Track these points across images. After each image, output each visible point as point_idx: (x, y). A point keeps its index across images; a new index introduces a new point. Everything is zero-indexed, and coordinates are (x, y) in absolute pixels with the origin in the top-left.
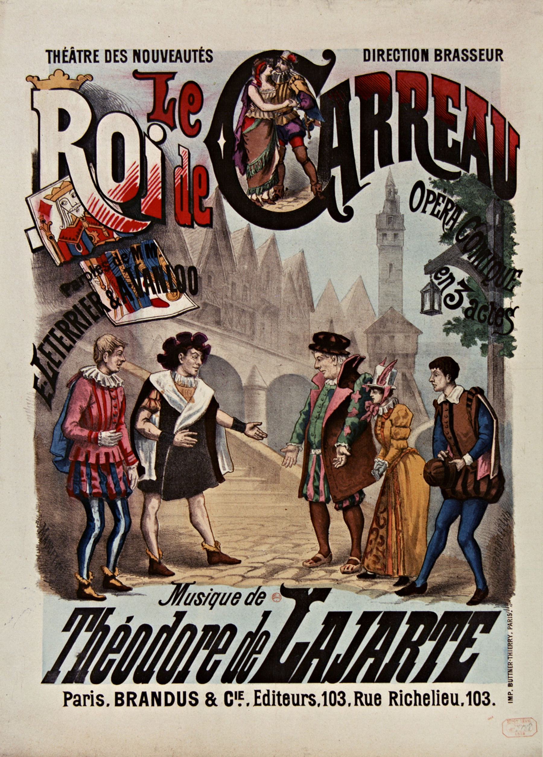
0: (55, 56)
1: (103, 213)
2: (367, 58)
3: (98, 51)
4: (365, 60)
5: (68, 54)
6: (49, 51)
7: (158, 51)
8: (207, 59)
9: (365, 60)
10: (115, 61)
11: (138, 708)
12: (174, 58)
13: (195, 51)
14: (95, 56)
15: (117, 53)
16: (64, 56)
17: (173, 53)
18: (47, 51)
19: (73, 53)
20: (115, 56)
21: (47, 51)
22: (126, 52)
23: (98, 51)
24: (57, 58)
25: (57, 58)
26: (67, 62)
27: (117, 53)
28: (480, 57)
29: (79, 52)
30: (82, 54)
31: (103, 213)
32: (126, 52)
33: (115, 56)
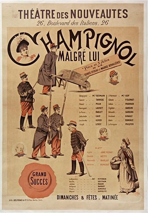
0: (25, 14)
1: (26, 105)
2: (59, 17)
3: (54, 10)
4: (58, 199)
5: (34, 13)
6: (21, 11)
7: (87, 10)
8: (65, 17)
9: (58, 199)
10: (62, 18)
11: (105, 200)
12: (33, 16)
13: (114, 10)
14: (53, 14)
15: (63, 14)
16: (32, 14)
17: (33, 12)
18: (19, 11)
19: (37, 12)
20: (62, 15)
21: (19, 11)
22: (68, 14)
23: (54, 10)
24: (26, 16)
25: (26, 16)
26: (33, 18)
27: (63, 14)
28: (62, 17)
29: (43, 11)
30: (45, 12)
31: (26, 105)
32: (68, 14)
33: (62, 15)
